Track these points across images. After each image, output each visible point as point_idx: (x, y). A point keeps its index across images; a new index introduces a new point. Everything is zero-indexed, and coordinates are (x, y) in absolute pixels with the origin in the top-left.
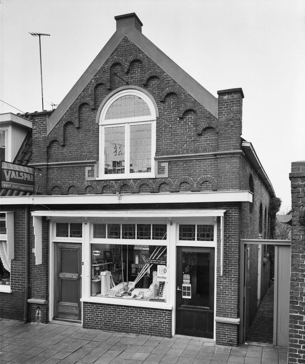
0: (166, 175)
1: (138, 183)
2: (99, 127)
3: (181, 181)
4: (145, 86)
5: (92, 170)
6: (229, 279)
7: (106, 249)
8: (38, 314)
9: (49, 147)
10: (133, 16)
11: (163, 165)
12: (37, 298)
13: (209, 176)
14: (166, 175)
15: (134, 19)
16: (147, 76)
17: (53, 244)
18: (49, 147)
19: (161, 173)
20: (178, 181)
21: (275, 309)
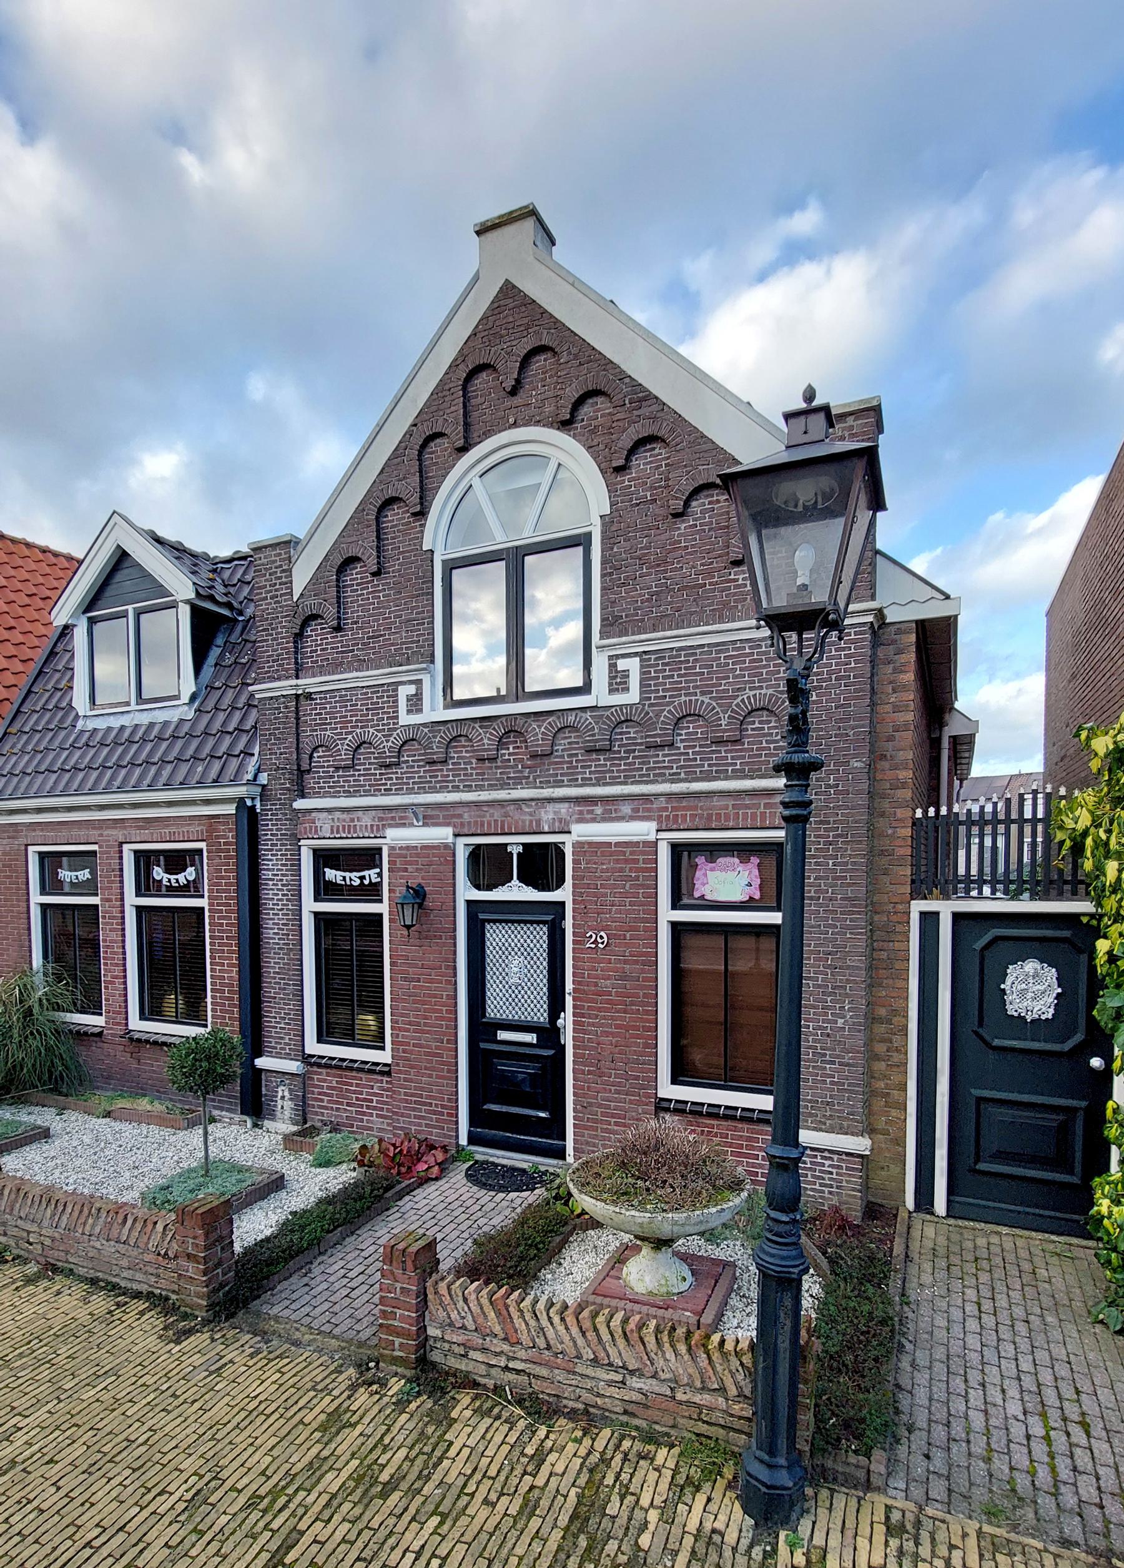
0: (633, 696)
1: (550, 723)
2: (299, 850)
3: (743, 710)
4: (565, 425)
5: (416, 695)
6: (397, 778)
7: (652, 1254)
8: (283, 1097)
9: (299, 636)
10: (531, 213)
11: (622, 664)
12: (278, 1056)
13: (771, 691)
14: (633, 696)
15: (529, 224)
16: (573, 392)
17: (312, 916)
18: (299, 636)
19: (618, 690)
20: (670, 712)
21: (943, 1096)
